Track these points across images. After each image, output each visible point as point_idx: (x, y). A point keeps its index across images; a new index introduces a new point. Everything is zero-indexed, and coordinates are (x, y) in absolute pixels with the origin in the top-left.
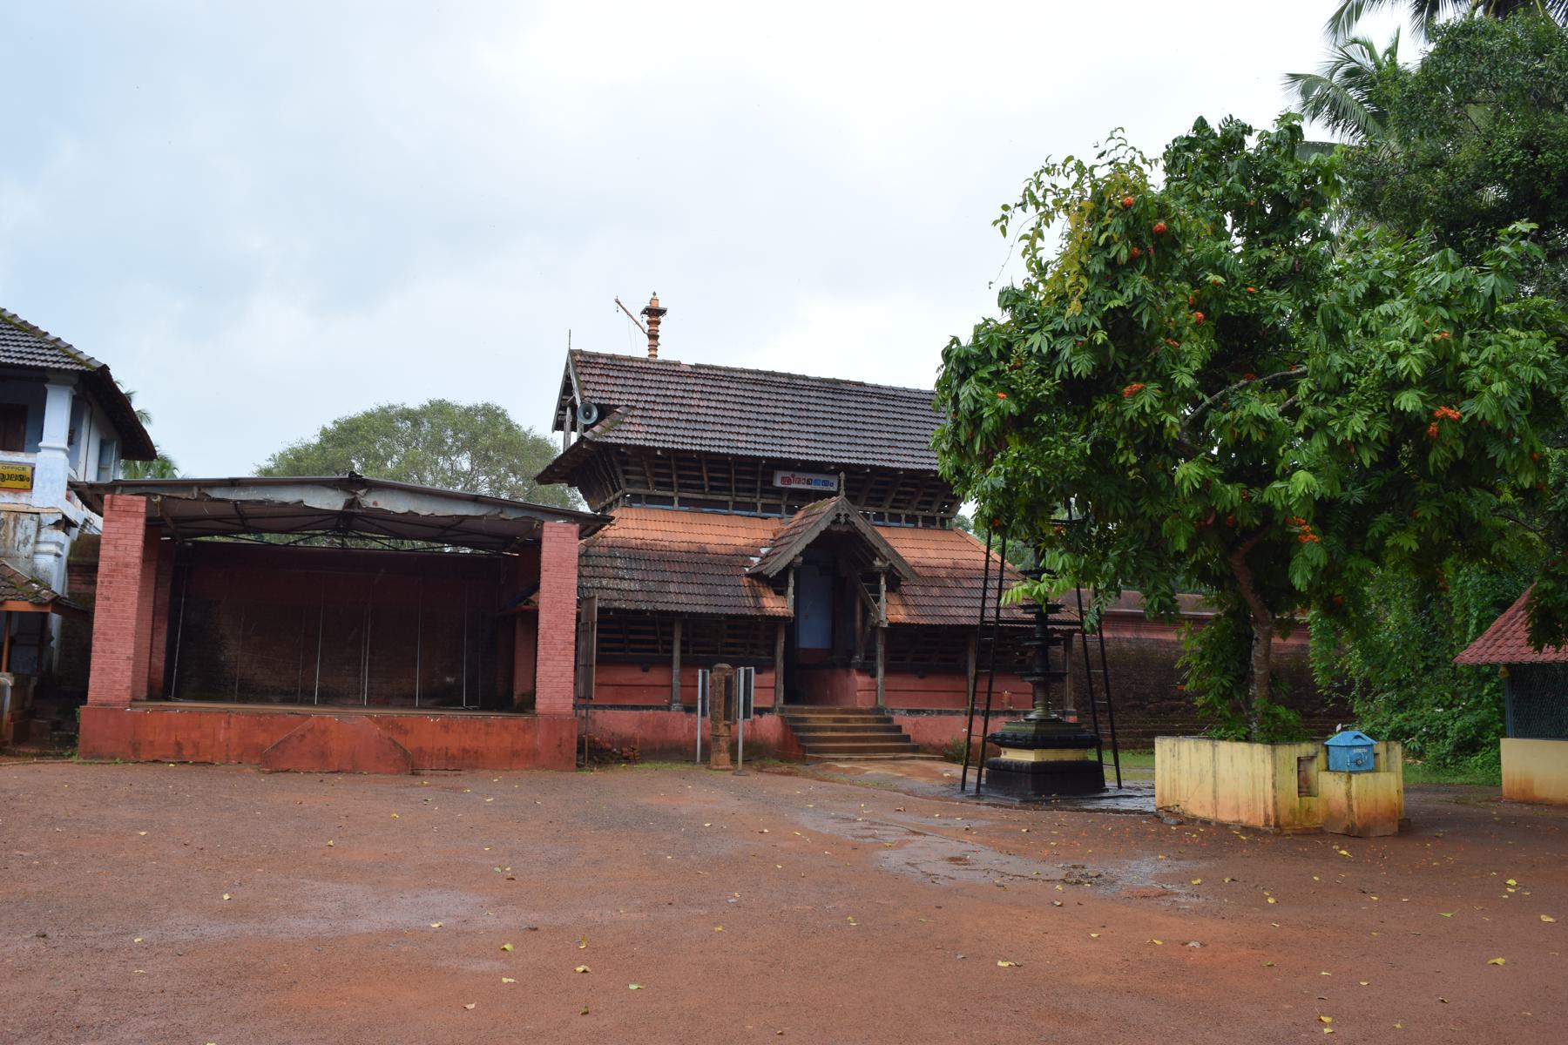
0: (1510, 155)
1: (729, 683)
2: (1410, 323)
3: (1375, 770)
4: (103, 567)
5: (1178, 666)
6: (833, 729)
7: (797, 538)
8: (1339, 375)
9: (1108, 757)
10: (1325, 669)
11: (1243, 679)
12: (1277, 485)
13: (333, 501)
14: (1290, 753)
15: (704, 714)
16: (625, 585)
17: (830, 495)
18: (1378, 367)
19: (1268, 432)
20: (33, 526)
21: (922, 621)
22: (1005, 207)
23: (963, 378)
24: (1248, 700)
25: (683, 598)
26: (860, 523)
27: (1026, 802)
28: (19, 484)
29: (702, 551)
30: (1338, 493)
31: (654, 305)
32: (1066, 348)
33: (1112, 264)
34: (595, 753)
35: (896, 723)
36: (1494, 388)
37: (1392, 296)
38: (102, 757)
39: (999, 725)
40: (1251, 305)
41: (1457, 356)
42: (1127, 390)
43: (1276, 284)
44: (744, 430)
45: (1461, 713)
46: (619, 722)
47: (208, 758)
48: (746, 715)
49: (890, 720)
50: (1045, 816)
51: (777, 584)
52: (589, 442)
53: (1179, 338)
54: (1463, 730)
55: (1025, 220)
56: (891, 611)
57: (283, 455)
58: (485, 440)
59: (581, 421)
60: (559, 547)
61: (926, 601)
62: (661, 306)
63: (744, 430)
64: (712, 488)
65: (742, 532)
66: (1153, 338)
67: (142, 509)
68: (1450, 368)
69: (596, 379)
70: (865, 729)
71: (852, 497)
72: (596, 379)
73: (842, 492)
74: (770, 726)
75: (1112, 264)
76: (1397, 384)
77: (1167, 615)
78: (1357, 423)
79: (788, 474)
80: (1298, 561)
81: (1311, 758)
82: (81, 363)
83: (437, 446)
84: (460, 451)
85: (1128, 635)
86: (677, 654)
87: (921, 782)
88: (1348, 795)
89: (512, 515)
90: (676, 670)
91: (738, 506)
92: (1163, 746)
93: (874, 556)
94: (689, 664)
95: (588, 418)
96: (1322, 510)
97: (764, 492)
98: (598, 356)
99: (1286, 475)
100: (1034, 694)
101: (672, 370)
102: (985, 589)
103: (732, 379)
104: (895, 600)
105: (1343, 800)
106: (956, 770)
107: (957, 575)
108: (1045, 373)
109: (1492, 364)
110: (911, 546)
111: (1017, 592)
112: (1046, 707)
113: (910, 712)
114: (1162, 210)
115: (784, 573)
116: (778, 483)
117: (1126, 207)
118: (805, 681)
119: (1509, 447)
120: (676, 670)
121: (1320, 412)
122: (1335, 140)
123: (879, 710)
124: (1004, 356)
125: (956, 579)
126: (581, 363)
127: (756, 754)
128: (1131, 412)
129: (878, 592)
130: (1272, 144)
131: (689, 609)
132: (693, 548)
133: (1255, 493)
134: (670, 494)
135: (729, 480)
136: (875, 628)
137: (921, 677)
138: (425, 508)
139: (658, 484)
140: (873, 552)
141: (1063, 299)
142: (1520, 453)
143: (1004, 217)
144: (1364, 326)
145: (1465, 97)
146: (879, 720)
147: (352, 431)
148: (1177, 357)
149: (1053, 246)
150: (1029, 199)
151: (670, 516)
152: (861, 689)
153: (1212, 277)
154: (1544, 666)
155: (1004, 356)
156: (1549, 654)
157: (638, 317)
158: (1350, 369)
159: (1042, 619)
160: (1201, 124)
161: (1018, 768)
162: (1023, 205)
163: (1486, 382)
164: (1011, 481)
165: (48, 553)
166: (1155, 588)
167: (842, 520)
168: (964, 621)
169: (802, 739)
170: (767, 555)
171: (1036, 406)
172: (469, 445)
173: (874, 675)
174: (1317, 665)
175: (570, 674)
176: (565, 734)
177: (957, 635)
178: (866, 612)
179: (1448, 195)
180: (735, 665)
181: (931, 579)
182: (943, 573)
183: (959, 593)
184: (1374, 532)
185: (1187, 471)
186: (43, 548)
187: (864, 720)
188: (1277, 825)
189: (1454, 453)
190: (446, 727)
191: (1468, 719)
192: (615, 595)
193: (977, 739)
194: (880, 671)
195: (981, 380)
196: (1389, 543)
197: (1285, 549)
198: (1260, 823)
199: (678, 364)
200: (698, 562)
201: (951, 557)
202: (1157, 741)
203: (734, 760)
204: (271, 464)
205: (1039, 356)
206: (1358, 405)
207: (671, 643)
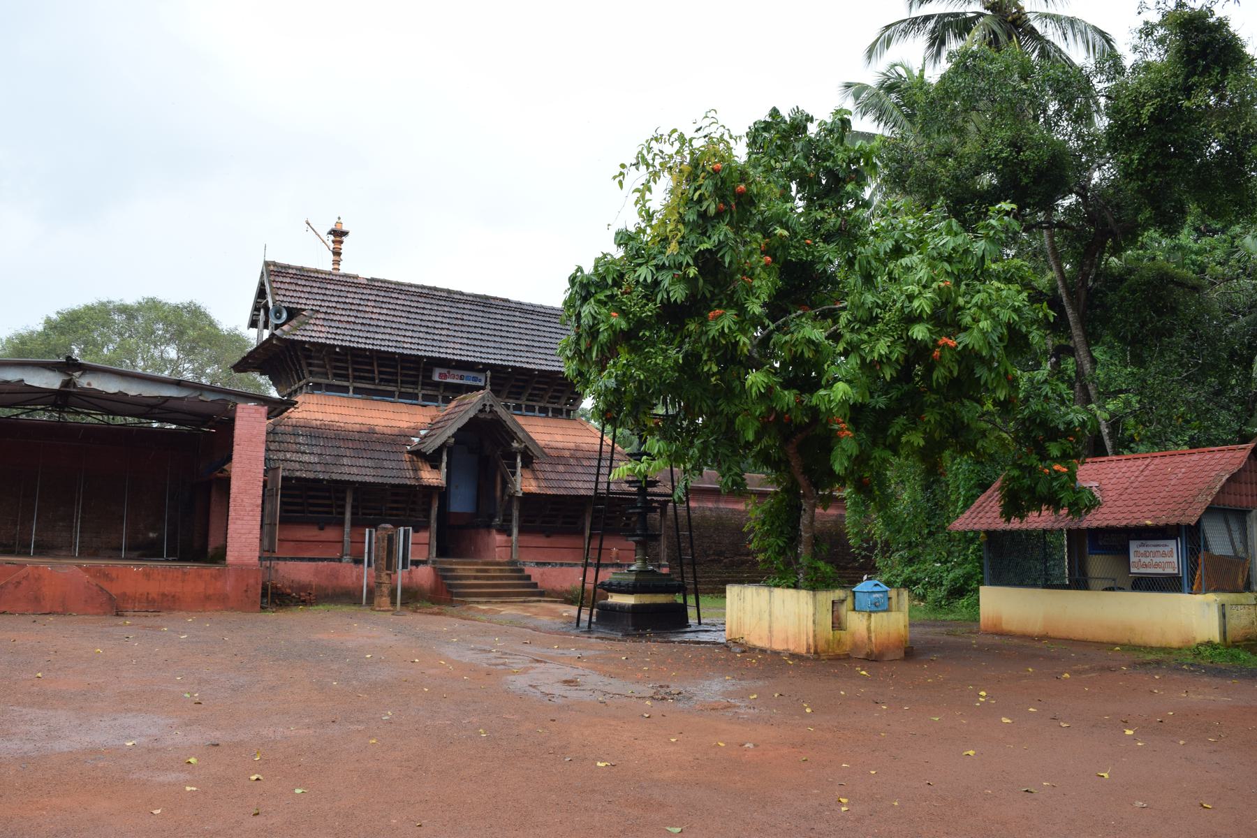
0: (1001, 151)
1: (391, 540)
2: (923, 273)
3: (888, 610)
5: (745, 529)
6: (476, 578)
8: (870, 310)
9: (691, 600)
11: (794, 540)
12: (822, 392)
14: (827, 597)
15: (369, 565)
16: (306, 458)
17: (478, 388)
18: (899, 305)
19: (817, 351)
22: (623, 166)
23: (585, 300)
24: (797, 556)
25: (355, 470)
29: (372, 432)
31: (338, 228)
32: (666, 279)
33: (703, 215)
34: (277, 597)
37: (911, 252)
39: (607, 575)
40: (808, 253)
41: (955, 300)
44: (410, 334)
45: (953, 567)
46: (298, 572)
48: (405, 566)
49: (522, 570)
51: (433, 460)
52: (279, 339)
54: (955, 580)
55: (637, 177)
56: (525, 483)
58: (191, 333)
59: (273, 321)
60: (250, 426)
61: (553, 476)
62: (344, 228)
63: (410, 334)
65: (405, 417)
66: (732, 275)
68: (951, 309)
69: (286, 286)
70: (501, 578)
71: (496, 391)
72: (286, 286)
73: (488, 387)
74: (424, 575)
75: (703, 215)
76: (911, 319)
77: (738, 490)
78: (882, 347)
79: (444, 371)
80: (837, 452)
81: (843, 601)
83: (148, 335)
85: (710, 505)
86: (348, 516)
87: (545, 620)
88: (869, 629)
89: (209, 397)
91: (402, 395)
93: (513, 439)
94: (358, 524)
95: (279, 318)
96: (856, 412)
98: (289, 267)
99: (829, 385)
101: (351, 282)
102: (599, 467)
103: (401, 292)
104: (528, 474)
105: (865, 633)
106: (573, 610)
107: (577, 456)
108: (649, 298)
110: (542, 432)
111: (623, 470)
112: (644, 561)
113: (537, 564)
114: (743, 176)
115: (439, 451)
116: (436, 378)
117: (716, 171)
118: (454, 539)
119: (991, 369)
121: (855, 337)
123: (513, 563)
124: (617, 284)
125: (577, 459)
126: (274, 271)
127: (412, 598)
129: (515, 468)
131: (359, 479)
132: (364, 429)
133: (806, 398)
134: (345, 384)
136: (512, 497)
139: (336, 376)
140: (512, 436)
141: (665, 241)
142: (998, 374)
143: (621, 174)
145: (970, 105)
146: (512, 571)
147: (73, 321)
148: (750, 291)
149: (659, 198)
150: (641, 160)
151: (346, 402)
152: (499, 546)
156: (1015, 524)
157: (325, 237)
158: (878, 306)
159: (642, 491)
160: (775, 112)
161: (621, 609)
162: (636, 165)
163: (976, 320)
164: (621, 382)
166: (729, 469)
167: (488, 409)
169: (450, 586)
170: (425, 436)
171: (641, 323)
172: (178, 336)
173: (510, 535)
174: (851, 530)
176: (252, 581)
178: (505, 483)
181: (557, 458)
182: (567, 454)
183: (580, 470)
184: (893, 431)
185: (755, 379)
187: (501, 570)
188: (816, 652)
189: (951, 372)
191: (959, 572)
193: (589, 586)
194: (515, 531)
195: (599, 301)
196: (904, 439)
197: (827, 442)
198: (803, 650)
199: (356, 277)
200: (367, 441)
201: (572, 443)
202: (728, 587)
203: (393, 603)
205: (645, 285)
206: (883, 333)
207: (343, 507)
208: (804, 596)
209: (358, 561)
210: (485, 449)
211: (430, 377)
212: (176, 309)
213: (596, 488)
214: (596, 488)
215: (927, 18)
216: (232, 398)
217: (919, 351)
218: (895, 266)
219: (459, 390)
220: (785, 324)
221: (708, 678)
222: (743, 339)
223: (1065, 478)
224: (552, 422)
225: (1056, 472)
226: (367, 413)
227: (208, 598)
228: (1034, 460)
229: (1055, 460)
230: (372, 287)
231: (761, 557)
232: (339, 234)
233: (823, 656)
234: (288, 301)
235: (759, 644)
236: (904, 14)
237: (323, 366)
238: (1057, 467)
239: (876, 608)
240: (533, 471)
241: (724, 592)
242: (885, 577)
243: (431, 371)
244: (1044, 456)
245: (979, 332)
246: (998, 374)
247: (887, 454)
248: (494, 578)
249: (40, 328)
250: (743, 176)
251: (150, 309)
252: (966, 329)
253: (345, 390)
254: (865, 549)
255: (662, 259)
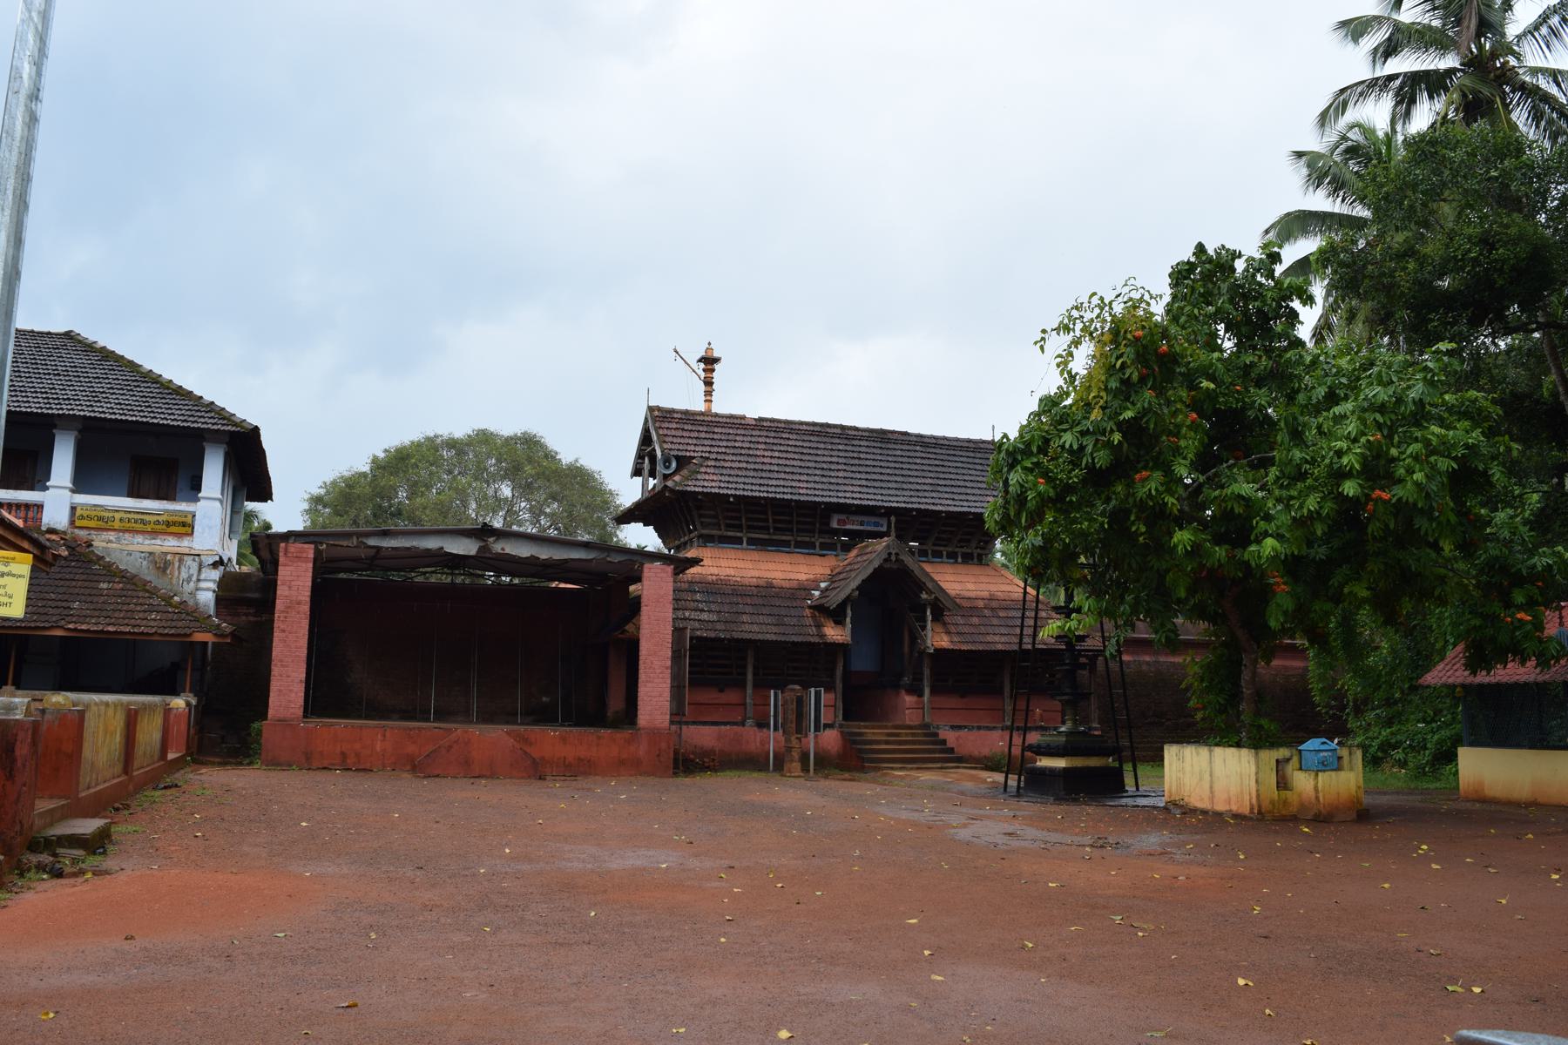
0: (1469, 251)
1: (800, 702)
2: (1352, 427)
3: (1339, 769)
4: (279, 604)
5: (1183, 686)
6: (887, 742)
7: (853, 574)
8: (1299, 467)
9: (1128, 767)
10: (1322, 690)
11: (1235, 697)
12: (1253, 548)
13: (464, 547)
14: (1270, 756)
15: (776, 729)
16: (705, 616)
17: (880, 535)
18: (1327, 461)
19: (1247, 506)
20: (195, 566)
21: (964, 647)
22: (1044, 331)
23: (1011, 467)
24: (1239, 715)
25: (755, 628)
26: (908, 560)
27: (1059, 800)
28: (182, 530)
29: (770, 586)
30: (1304, 551)
32: (1089, 443)
33: (1126, 382)
34: (687, 763)
35: (941, 737)
36: (1415, 477)
37: (1346, 398)
38: (279, 764)
39: (1034, 738)
40: (1238, 401)
41: (1388, 452)
42: (1137, 476)
43: (1259, 385)
44: (804, 478)
45: (1439, 728)
46: (703, 736)
47: (368, 766)
48: (817, 729)
49: (936, 735)
50: (1075, 809)
51: (837, 616)
52: (672, 490)
53: (1177, 435)
54: (1440, 742)
55: (1058, 343)
56: (937, 639)
57: (334, 483)
59: (660, 468)
60: (655, 588)
61: (966, 629)
62: (716, 355)
63: (804, 478)
64: (776, 529)
65: (803, 569)
66: (1157, 438)
67: (311, 556)
68: (1383, 462)
69: (674, 433)
70: (914, 743)
71: (902, 537)
72: (674, 433)
73: (893, 534)
74: (831, 739)
75: (1126, 382)
76: (1341, 475)
77: (1174, 644)
78: (1312, 503)
79: (843, 517)
80: (1272, 608)
81: (1288, 760)
82: (236, 424)
83: (480, 473)
84: (503, 479)
85: (1147, 658)
86: (750, 677)
87: (968, 785)
88: (1316, 788)
89: (616, 558)
90: (749, 691)
91: (799, 545)
92: (1171, 753)
94: (762, 685)
95: (668, 468)
96: (1292, 566)
97: (821, 532)
98: (674, 411)
99: (1258, 542)
100: (1063, 715)
101: (736, 423)
102: (1023, 618)
103: (791, 431)
104: (939, 629)
105: (1312, 794)
106: (999, 777)
107: (994, 606)
108: (1075, 464)
109: (1416, 458)
110: (955, 581)
111: (1052, 628)
112: (1075, 722)
113: (953, 727)
114: (1165, 334)
115: (842, 606)
116: (835, 525)
117: (1137, 339)
118: (861, 701)
119: (1431, 519)
120: (749, 691)
121: (1284, 493)
122: (1337, 210)
123: (926, 726)
124: (1043, 450)
125: (993, 609)
126: (659, 418)
127: (825, 764)
128: (1141, 492)
129: (925, 621)
130: (1253, 267)
131: (760, 637)
132: (762, 583)
133: (1238, 552)
135: (790, 522)
136: (922, 653)
137: (962, 696)
138: (544, 553)
139: (728, 526)
140: (921, 587)
141: (1088, 407)
142: (1439, 523)
143: (1043, 339)
144: (1319, 427)
145: (1435, 194)
146: (926, 735)
148: (1177, 451)
149: (1081, 362)
150: (1064, 328)
151: (740, 554)
152: (909, 707)
153: (1205, 384)
154: (1481, 686)
155: (1043, 450)
156: (1482, 678)
157: (694, 365)
158: (1307, 462)
159: (1070, 645)
160: (1200, 249)
161: (1051, 772)
162: (1057, 330)
163: (1410, 471)
164: (1048, 540)
165: (208, 589)
166: (1163, 625)
168: (1000, 647)
169: (860, 751)
170: (827, 589)
171: (1069, 489)
172: (512, 473)
173: (921, 695)
174: (1315, 686)
175: (667, 695)
176: (664, 745)
177: (996, 659)
178: (914, 639)
179: (1416, 282)
180: (806, 687)
181: (969, 609)
182: (981, 604)
183: (995, 621)
184: (1334, 582)
185: (1182, 538)
186: (203, 585)
187: (913, 735)
188: (1260, 812)
189: (1387, 525)
190: (563, 739)
191: (1445, 733)
192: (697, 625)
193: (1016, 751)
194: (927, 691)
195: (1025, 469)
196: (1346, 590)
197: (1265, 594)
198: (1246, 811)
199: (743, 418)
200: (766, 594)
201: (987, 587)
202: (1166, 747)
203: (805, 769)
204: (322, 491)
205: (1071, 451)
206: (1312, 489)
207: (745, 667)
208: (1246, 755)
209: (762, 724)
210: (892, 601)
211: (828, 524)
212: (510, 441)
213: (1021, 643)
214: (1021, 643)
215: (1391, 78)
216: (639, 558)
217: (1349, 512)
218: (1324, 418)
219: (857, 537)
220: (1215, 475)
221: (1146, 832)
222: (1170, 500)
223: (1529, 627)
224: (962, 568)
225: (1520, 620)
226: (763, 566)
227: (622, 762)
228: (1496, 607)
229: (1520, 608)
230: (761, 428)
231: (1199, 716)
232: (709, 361)
233: (1268, 817)
234: (676, 449)
235: (1200, 805)
236: (1367, 75)
237: (715, 517)
238: (1520, 615)
239: (1324, 766)
240: (945, 624)
241: (1162, 759)
242: (1359, 740)
243: (829, 518)
244: (1508, 604)
245: (1413, 481)
246: (1439, 523)
247: (1328, 606)
248: (906, 742)
249: (366, 469)
250: (1165, 334)
251: (480, 442)
252: (1400, 481)
253: (739, 541)
254: (1332, 708)
255: (1087, 425)
